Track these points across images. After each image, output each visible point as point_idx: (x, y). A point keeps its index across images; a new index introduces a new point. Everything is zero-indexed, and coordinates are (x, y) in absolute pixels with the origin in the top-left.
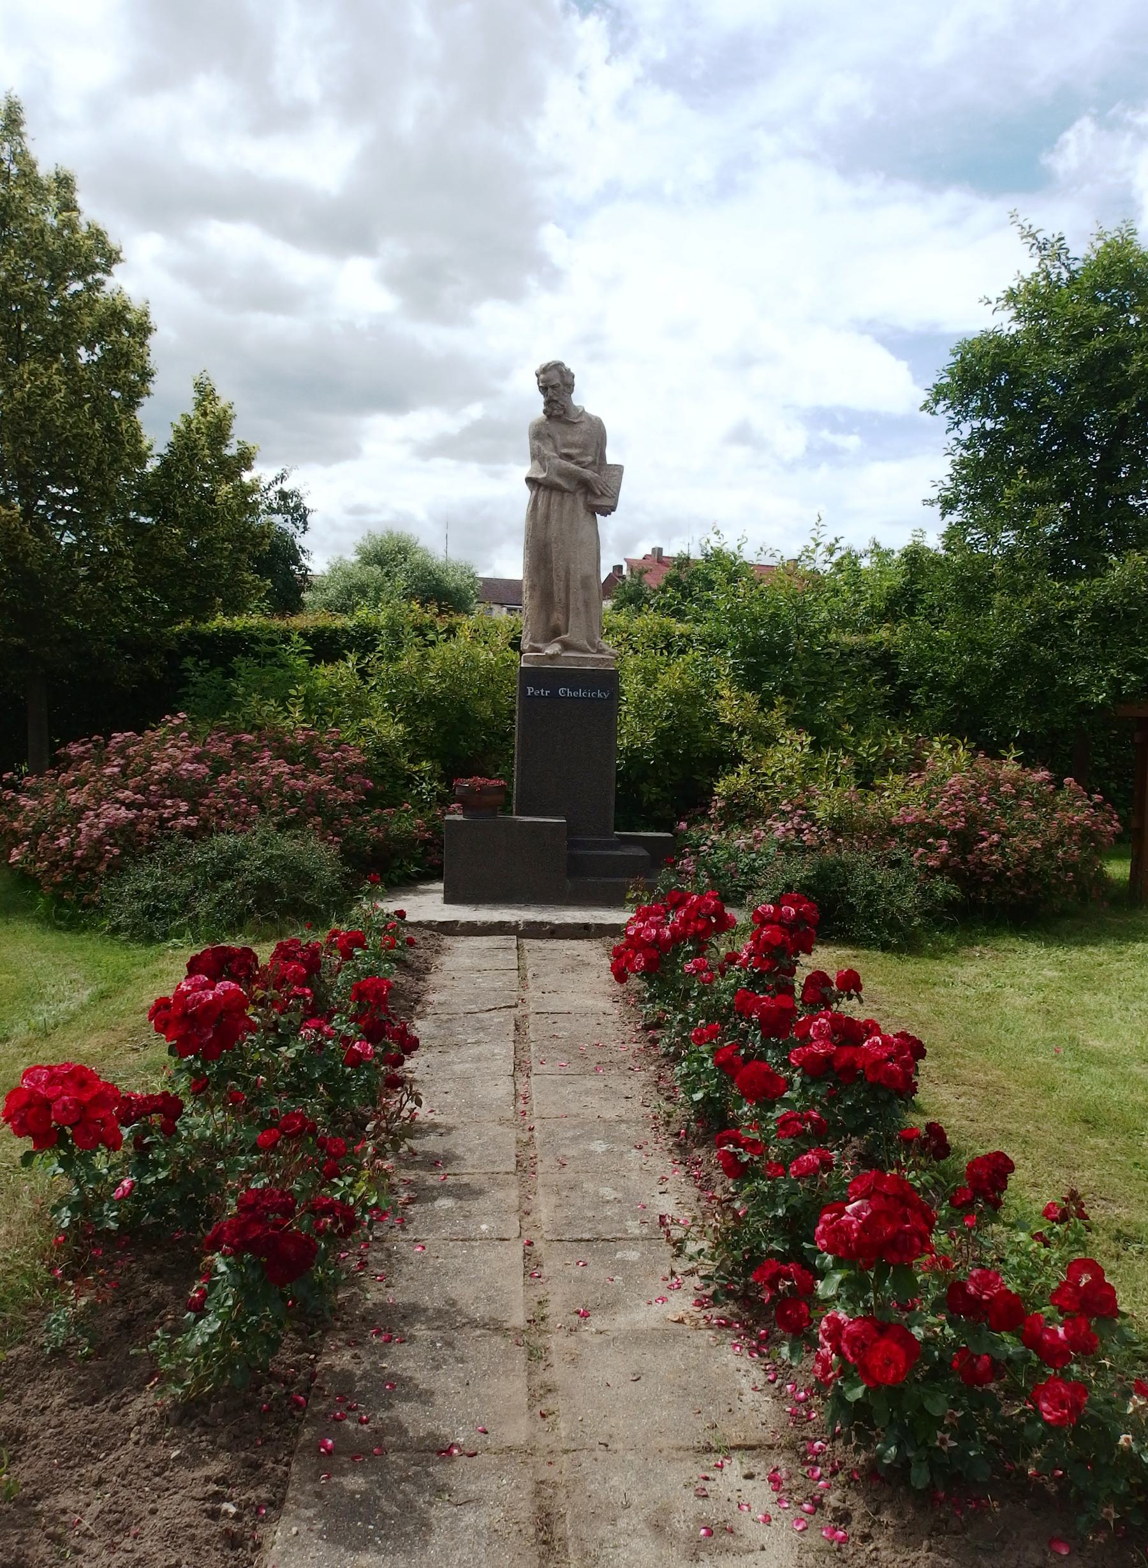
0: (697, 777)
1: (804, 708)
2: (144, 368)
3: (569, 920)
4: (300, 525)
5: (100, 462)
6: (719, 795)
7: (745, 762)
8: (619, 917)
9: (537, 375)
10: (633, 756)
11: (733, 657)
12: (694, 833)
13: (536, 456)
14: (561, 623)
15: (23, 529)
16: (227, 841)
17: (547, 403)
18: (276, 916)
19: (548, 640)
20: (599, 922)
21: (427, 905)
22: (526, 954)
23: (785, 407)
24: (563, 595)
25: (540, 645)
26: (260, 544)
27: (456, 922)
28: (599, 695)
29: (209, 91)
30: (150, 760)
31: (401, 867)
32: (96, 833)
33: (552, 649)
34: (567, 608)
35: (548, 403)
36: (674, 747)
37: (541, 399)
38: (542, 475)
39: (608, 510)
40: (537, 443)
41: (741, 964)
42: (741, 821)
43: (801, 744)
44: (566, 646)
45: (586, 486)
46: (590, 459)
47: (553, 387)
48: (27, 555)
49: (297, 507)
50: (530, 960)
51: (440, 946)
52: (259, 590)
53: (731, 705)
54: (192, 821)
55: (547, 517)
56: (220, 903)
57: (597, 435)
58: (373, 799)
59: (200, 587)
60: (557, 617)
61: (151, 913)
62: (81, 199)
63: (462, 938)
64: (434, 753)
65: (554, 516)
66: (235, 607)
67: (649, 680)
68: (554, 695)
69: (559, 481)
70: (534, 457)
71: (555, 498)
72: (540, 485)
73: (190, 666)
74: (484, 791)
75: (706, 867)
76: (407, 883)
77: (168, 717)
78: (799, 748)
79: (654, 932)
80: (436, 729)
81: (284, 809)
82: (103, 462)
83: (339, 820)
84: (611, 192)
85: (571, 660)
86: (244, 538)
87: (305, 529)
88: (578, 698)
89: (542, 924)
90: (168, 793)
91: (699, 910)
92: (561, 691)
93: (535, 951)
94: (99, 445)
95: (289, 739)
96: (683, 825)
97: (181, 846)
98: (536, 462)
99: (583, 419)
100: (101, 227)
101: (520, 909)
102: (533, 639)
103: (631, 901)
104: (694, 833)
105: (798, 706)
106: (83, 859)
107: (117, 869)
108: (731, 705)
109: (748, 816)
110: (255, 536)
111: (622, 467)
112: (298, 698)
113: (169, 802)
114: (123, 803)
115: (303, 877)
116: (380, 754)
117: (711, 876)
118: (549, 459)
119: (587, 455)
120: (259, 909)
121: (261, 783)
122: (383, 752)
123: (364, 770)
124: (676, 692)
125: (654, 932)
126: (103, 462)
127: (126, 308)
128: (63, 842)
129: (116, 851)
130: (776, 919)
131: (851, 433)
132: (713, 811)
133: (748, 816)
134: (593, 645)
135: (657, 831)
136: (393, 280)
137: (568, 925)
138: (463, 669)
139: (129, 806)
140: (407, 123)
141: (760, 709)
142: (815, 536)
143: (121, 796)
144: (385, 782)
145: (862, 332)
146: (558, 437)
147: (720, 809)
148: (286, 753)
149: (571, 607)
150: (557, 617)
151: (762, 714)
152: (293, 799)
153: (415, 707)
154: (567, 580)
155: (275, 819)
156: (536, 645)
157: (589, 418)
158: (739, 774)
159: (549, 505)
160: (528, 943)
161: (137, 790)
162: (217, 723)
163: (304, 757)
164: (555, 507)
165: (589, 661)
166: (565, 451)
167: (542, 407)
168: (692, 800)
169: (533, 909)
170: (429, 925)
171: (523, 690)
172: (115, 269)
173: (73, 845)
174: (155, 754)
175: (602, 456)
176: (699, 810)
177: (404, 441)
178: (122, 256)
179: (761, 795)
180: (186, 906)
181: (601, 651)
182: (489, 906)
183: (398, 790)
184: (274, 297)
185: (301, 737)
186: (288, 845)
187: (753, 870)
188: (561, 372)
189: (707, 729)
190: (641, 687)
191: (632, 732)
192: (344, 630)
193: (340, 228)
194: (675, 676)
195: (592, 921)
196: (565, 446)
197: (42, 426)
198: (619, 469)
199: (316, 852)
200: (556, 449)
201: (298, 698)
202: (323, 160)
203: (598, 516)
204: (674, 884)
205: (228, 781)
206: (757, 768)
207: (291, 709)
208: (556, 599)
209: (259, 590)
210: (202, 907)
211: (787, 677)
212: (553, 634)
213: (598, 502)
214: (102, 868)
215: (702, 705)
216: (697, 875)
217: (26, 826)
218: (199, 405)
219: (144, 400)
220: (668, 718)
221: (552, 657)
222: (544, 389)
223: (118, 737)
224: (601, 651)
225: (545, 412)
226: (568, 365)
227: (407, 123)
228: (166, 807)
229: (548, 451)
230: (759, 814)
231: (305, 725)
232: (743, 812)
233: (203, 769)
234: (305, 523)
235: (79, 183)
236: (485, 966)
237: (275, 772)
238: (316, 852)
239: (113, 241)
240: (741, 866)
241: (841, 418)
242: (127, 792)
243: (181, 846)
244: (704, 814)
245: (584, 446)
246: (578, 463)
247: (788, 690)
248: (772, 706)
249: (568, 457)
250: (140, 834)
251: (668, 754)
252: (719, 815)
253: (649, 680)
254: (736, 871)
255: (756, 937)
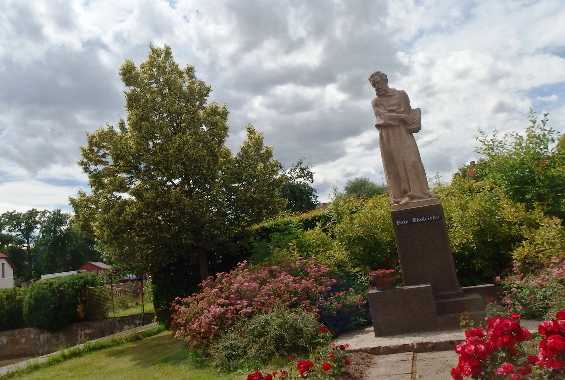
0: (502, 252)
1: (552, 205)
2: (224, 127)
3: (442, 340)
4: (310, 179)
5: (209, 165)
6: (516, 259)
7: (526, 239)
8: (461, 335)
9: (370, 80)
10: (464, 247)
11: (506, 187)
12: (506, 282)
13: (378, 114)
14: (407, 187)
15: (182, 196)
16: (261, 318)
17: (377, 90)
18: (286, 353)
19: (402, 197)
20: (459, 339)
21: (367, 340)
22: (417, 363)
23: (517, 92)
24: (404, 174)
25: (398, 200)
26: (280, 186)
27: (380, 347)
28: (434, 218)
29: (269, 44)
30: (231, 284)
31: (355, 320)
32: (208, 320)
34: (408, 178)
35: (377, 90)
36: (485, 238)
37: (374, 90)
38: (382, 122)
39: (418, 130)
40: (376, 109)
41: (539, 364)
42: (533, 271)
43: (555, 224)
44: (412, 198)
45: (403, 122)
46: (403, 109)
47: (377, 83)
48: (185, 206)
49: (308, 173)
50: (419, 365)
51: (370, 362)
52: (283, 204)
53: (509, 211)
54: (250, 310)
55: (388, 140)
56: (260, 349)
57: (404, 97)
58: (336, 288)
59: (257, 207)
60: (404, 185)
61: (229, 358)
62: (196, 74)
63: (384, 356)
64: (366, 262)
65: (392, 141)
66: (273, 213)
67: (464, 207)
68: (411, 223)
69: (390, 122)
70: (377, 115)
71: (390, 130)
73: (253, 240)
74: (384, 276)
75: (518, 300)
76: (359, 328)
77: (239, 263)
78: (555, 226)
79: (473, 347)
80: (364, 251)
81: (291, 298)
82: (211, 165)
83: (318, 300)
84: (421, 33)
85: (416, 204)
86: (274, 184)
87: (313, 181)
88: (423, 222)
89: (427, 343)
90: (239, 297)
91: (502, 328)
92: (414, 220)
93: (423, 360)
94: (207, 158)
95: (293, 265)
96: (498, 278)
97: (244, 322)
98: (378, 117)
99: (395, 93)
100: (202, 81)
101: (415, 336)
102: (395, 198)
103: (464, 327)
104: (506, 282)
105: (549, 205)
106: (204, 332)
107: (217, 336)
108: (509, 211)
109: (537, 268)
110: (277, 183)
111: (419, 109)
112: (293, 246)
113: (239, 302)
114: (219, 305)
115: (298, 332)
116: (339, 266)
117: (523, 305)
118: (383, 114)
119: (401, 108)
120: (277, 351)
121: (280, 287)
122: (340, 265)
123: (330, 275)
124: (479, 211)
125: (473, 347)
126: (211, 165)
127: (217, 107)
128: (195, 326)
129: (216, 328)
130: (556, 330)
131: (552, 95)
132: (515, 268)
133: (537, 268)
134: (425, 194)
135: (488, 284)
136: (344, 89)
137: (441, 343)
138: (372, 220)
139: (222, 306)
140: (338, 33)
141: (527, 211)
142: (531, 118)
143: (218, 301)
144: (342, 280)
145: (545, 53)
146: (385, 103)
147: (519, 267)
148: (293, 272)
149: (410, 179)
150: (404, 185)
151: (528, 213)
152: (296, 293)
153: (353, 242)
154: (405, 167)
155: (286, 304)
156: (397, 200)
157: (398, 92)
158: (523, 247)
159: (388, 134)
160: (420, 356)
161: (227, 298)
162: (264, 263)
163: (299, 273)
164: (391, 135)
165: (424, 203)
166: (390, 108)
167: (375, 93)
168: (503, 265)
169: (422, 335)
170: (366, 351)
171: (395, 223)
172: (210, 94)
173: (200, 327)
174: (233, 281)
175: (409, 107)
176: (507, 270)
177: (361, 145)
178: (211, 89)
179: (540, 255)
180: (245, 352)
181: (430, 197)
182: (435, 331)
183: (351, 282)
184: (302, 106)
185: (298, 264)
186: (290, 316)
187: (545, 298)
188: (380, 75)
189: (501, 226)
190: (461, 213)
191: (459, 236)
192: (324, 216)
193: (321, 77)
194: (476, 204)
195: (455, 339)
196: (390, 106)
197: (185, 156)
198: (418, 111)
199: (307, 319)
200: (385, 109)
201: (293, 246)
202: (312, 56)
204: (495, 312)
205: (265, 289)
206: (534, 241)
207: (292, 251)
208: (402, 177)
209: (283, 204)
210: (252, 352)
211: (538, 190)
212: (404, 193)
213: (411, 127)
214: (211, 337)
215: (495, 215)
216: (514, 305)
217: (183, 320)
218: (249, 136)
219: (226, 139)
220: (478, 225)
221: (405, 204)
222: (374, 85)
223: (218, 275)
224: (430, 197)
225: (377, 94)
226: (382, 72)
227: (338, 33)
228: (238, 304)
229: (382, 111)
230: (541, 266)
231: (300, 258)
232: (532, 266)
233: (255, 285)
234: (312, 179)
235: (196, 69)
236: (394, 372)
237: (285, 281)
238: (307, 319)
239: (207, 84)
240: (538, 296)
241: (546, 90)
242: (222, 300)
243: (244, 322)
244: (511, 272)
245: (399, 105)
246: (397, 113)
247: (540, 198)
248: (533, 208)
249: (392, 111)
250: (228, 319)
251: (484, 243)
252: (520, 270)
253: (464, 207)
254: (536, 300)
255: (543, 344)
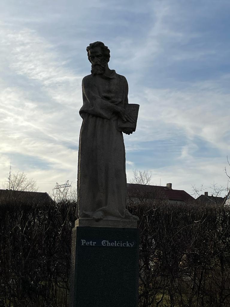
28: (128, 245)
33: (98, 214)
39: (131, 130)
45: (117, 114)
46: (120, 100)
57: (122, 84)
72: (89, 114)
88: (114, 247)
92: (103, 242)
156: (87, 213)
175: (127, 100)
203: (124, 134)
246: (113, 102)
249: (107, 98)
